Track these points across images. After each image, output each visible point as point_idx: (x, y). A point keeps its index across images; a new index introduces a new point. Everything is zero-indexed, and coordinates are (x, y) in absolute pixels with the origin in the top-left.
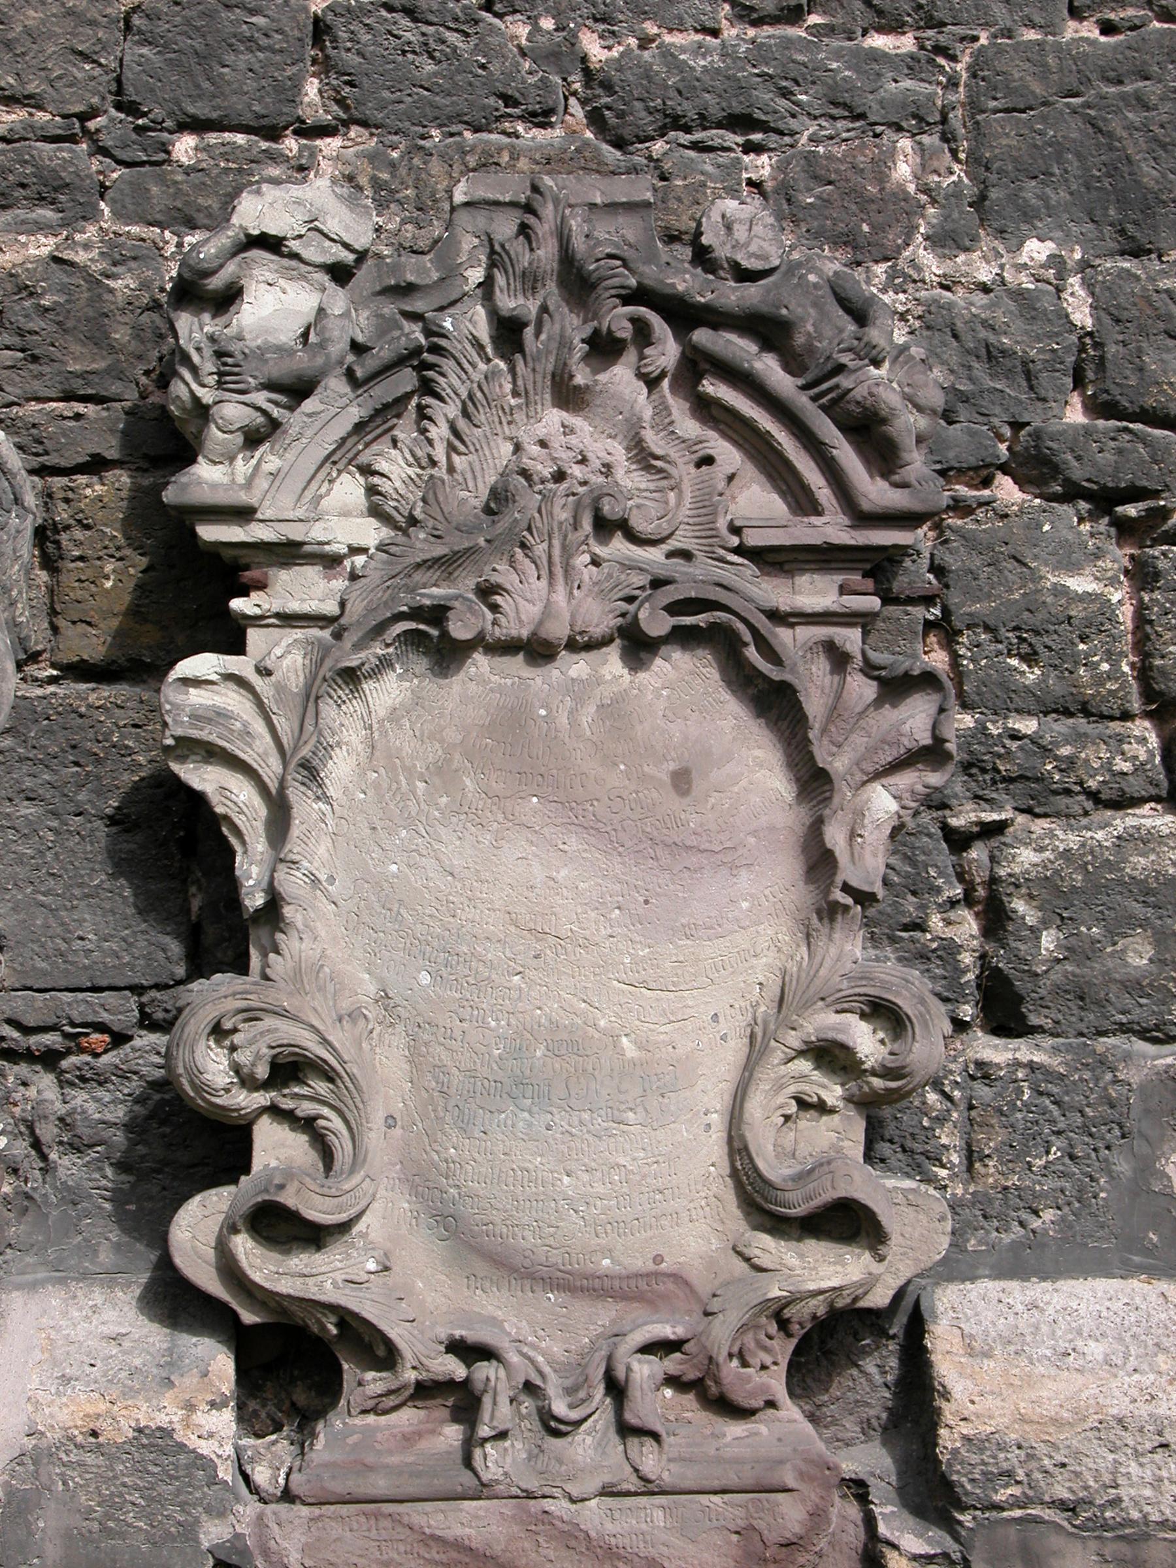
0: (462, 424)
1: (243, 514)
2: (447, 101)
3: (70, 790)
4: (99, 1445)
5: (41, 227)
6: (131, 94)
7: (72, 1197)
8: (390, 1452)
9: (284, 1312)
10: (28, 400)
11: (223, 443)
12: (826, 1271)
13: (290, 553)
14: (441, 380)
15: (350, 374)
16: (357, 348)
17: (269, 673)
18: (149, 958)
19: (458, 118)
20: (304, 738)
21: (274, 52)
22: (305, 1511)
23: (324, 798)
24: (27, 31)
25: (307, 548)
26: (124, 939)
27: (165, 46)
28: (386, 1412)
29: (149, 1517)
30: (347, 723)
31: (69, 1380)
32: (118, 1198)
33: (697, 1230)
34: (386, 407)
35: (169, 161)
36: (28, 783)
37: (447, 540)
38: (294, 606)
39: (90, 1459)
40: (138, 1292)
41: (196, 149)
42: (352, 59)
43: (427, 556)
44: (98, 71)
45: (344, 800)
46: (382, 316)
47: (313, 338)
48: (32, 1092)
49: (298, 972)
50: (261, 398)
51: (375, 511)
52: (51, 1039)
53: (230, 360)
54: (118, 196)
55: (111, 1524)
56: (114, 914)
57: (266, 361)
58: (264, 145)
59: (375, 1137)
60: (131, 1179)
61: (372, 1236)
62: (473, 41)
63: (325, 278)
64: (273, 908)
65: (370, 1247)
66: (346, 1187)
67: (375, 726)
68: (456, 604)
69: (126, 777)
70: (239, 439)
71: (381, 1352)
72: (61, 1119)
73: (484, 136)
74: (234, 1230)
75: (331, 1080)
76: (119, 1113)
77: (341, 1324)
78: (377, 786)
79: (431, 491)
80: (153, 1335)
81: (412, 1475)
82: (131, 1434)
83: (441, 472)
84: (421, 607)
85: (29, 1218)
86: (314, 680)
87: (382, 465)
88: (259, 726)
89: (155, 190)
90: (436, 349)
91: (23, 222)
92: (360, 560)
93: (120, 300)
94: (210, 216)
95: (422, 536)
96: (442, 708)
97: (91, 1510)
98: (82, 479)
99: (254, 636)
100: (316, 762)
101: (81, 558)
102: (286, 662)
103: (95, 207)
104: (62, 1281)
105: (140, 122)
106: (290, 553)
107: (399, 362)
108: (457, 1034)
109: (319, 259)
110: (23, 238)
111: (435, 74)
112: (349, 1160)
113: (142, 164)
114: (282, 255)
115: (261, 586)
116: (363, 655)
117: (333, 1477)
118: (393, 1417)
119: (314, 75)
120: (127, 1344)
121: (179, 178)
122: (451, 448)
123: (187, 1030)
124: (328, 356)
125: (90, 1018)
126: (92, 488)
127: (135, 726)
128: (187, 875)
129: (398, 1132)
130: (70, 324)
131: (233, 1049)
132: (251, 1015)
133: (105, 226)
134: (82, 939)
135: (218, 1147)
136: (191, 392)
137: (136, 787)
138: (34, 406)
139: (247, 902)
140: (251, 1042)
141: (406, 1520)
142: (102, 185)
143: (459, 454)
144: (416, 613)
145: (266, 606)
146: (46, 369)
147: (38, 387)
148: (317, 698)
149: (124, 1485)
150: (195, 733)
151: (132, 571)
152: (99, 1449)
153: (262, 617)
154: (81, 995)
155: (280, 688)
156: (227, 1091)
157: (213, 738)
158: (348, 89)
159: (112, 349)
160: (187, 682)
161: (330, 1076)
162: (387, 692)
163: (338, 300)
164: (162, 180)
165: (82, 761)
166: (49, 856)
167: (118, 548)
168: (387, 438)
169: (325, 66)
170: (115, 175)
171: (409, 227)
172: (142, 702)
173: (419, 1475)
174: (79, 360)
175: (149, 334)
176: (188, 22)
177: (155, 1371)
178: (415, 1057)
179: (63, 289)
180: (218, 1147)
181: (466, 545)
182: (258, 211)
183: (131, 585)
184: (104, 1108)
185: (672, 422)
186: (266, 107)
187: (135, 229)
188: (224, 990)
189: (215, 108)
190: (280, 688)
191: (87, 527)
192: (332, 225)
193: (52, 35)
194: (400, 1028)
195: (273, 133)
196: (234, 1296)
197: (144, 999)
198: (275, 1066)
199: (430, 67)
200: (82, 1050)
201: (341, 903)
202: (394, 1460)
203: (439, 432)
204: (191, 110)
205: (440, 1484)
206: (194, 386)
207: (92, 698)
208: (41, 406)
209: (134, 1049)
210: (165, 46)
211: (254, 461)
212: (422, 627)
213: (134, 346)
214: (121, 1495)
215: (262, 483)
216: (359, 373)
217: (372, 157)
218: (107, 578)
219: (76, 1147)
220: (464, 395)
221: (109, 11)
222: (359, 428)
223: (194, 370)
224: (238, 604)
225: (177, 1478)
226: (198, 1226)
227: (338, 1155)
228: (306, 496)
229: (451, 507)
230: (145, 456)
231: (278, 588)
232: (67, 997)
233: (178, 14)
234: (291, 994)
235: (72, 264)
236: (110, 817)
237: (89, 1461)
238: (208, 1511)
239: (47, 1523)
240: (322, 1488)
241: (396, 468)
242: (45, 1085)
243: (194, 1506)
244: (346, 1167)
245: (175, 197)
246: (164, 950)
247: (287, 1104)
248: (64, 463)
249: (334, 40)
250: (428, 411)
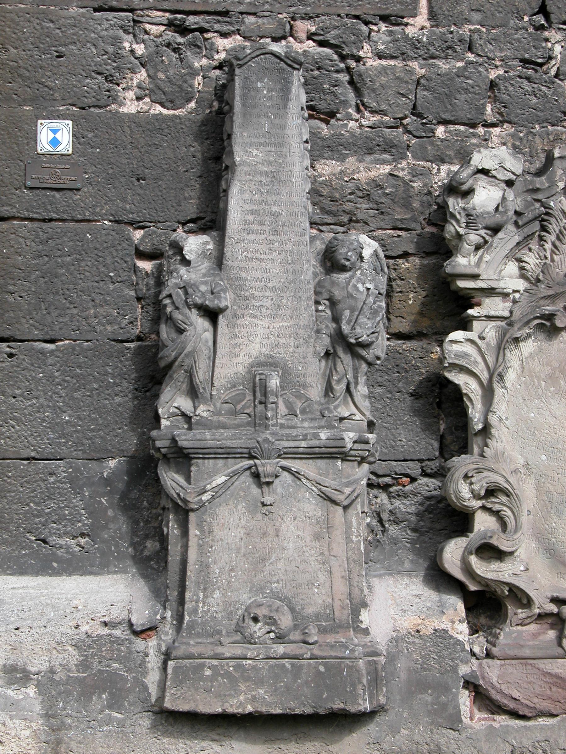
0: (558, 243)
1: (475, 277)
2: (542, 114)
3: (396, 382)
4: (420, 636)
5: (384, 162)
6: (420, 109)
7: (394, 541)
8: (529, 640)
9: (487, 585)
10: (378, 229)
11: (468, 250)
13: (491, 292)
14: (550, 226)
15: (516, 223)
16: (517, 213)
17: (484, 339)
18: (426, 448)
19: (546, 121)
20: (499, 364)
21: (475, 94)
22: (499, 662)
23: (505, 387)
24: (382, 86)
25: (497, 290)
26: (416, 441)
27: (434, 91)
28: (525, 625)
29: (440, 664)
30: (513, 357)
31: (405, 611)
32: (413, 542)
34: (528, 236)
35: (434, 137)
36: (380, 379)
37: (554, 288)
38: (492, 313)
39: (417, 641)
40: (421, 579)
41: (445, 132)
42: (506, 97)
43: (546, 295)
44: (408, 101)
45: (512, 388)
46: (527, 201)
47: (501, 209)
48: (379, 500)
49: (496, 454)
50: (483, 232)
51: (523, 276)
52: (387, 480)
53: (472, 218)
54: (414, 150)
55: (425, 666)
56: (413, 431)
57: (485, 218)
58: (471, 130)
59: (524, 519)
60: (417, 535)
61: (522, 557)
62: (552, 90)
63: (503, 185)
64: (486, 431)
65: (521, 561)
66: (515, 537)
67: (524, 360)
68: (558, 313)
69: (417, 378)
70: (473, 248)
71: (525, 601)
72: (390, 511)
73: (556, 128)
74: (471, 554)
75: (508, 496)
76: (413, 509)
77: (510, 591)
78: (525, 383)
79: (545, 269)
80: (430, 596)
81: (538, 649)
82: (432, 632)
83: (548, 261)
84: (544, 315)
85: (378, 549)
86: (502, 341)
87: (526, 259)
88: (479, 359)
89: (429, 148)
90: (547, 214)
91: (378, 160)
92: (517, 295)
93: (416, 191)
94: (450, 158)
95: (543, 286)
96: (550, 353)
97: (418, 660)
98: (401, 261)
99: (475, 324)
100: (503, 374)
101: (400, 292)
102: (489, 334)
103: (406, 154)
104: (391, 574)
105: (424, 121)
106: (491, 292)
107: (535, 219)
108: (556, 479)
109: (503, 178)
110: (378, 166)
111: (537, 103)
112: (514, 527)
113: (423, 137)
114: (489, 176)
115: (479, 305)
116: (521, 332)
117: (509, 649)
118: (528, 627)
119: (489, 102)
120: (423, 598)
121: (439, 143)
122: (553, 252)
123: (454, 476)
124: (508, 216)
125: (403, 472)
126: (404, 264)
127: (421, 358)
129: (531, 517)
130: (396, 200)
131: (471, 484)
132: (479, 471)
133: (410, 161)
134: (400, 441)
135: (461, 522)
136: (456, 229)
137: (421, 382)
138: (380, 232)
139: (475, 427)
140: (480, 481)
141: (537, 666)
142: (408, 146)
143: (556, 255)
144: (542, 317)
145: (481, 313)
146: (386, 217)
147: (382, 224)
148: (504, 349)
149: (430, 651)
150: (457, 362)
151: (420, 297)
152: (420, 637)
153: (480, 317)
154: (399, 463)
155: (488, 345)
156: (469, 500)
157: (464, 364)
158: (503, 109)
159: (412, 210)
160: (452, 341)
161: (507, 494)
162: (529, 347)
163: (510, 195)
164: (432, 144)
165: (400, 371)
166: (388, 408)
167: (415, 288)
168: (527, 248)
169: (495, 99)
170: (413, 142)
171: (527, 163)
172: (423, 348)
173: (541, 649)
174: (400, 214)
175: (426, 204)
176: (443, 82)
177: (437, 608)
178: (538, 488)
179: (394, 186)
180: (461, 522)
181: (561, 290)
182: (479, 159)
183: (419, 303)
184: (407, 507)
186: (472, 116)
187: (421, 163)
188: (468, 461)
189: (452, 116)
190: (488, 345)
191: (403, 280)
192: (508, 165)
193: (390, 87)
194: (533, 477)
195: (473, 126)
196: (468, 580)
197: (423, 464)
198: (487, 490)
199: (535, 100)
200: (399, 484)
201: (510, 428)
202: (531, 643)
203: (548, 246)
204: (444, 117)
205: (549, 652)
206: (457, 227)
207: (404, 346)
208: (384, 232)
209: (419, 484)
210: (434, 91)
211: (478, 257)
212: (543, 322)
213: (420, 209)
214: (429, 655)
215: (483, 265)
216: (520, 223)
217: (513, 136)
218: (410, 300)
219: (396, 522)
220: (557, 232)
221: (413, 77)
222: (518, 243)
223: (458, 221)
224: (470, 312)
225: (450, 649)
226: (453, 553)
227: (509, 525)
228: (494, 269)
229: (554, 275)
230: (424, 252)
231: (485, 305)
232: (394, 463)
233: (439, 79)
234: (494, 463)
235: (398, 176)
236: (411, 393)
237: (417, 642)
238: (462, 661)
239: (401, 665)
240: (505, 653)
241: (532, 260)
242: (383, 497)
243: (456, 659)
244: (513, 530)
245: (437, 150)
246: (432, 446)
247: (489, 506)
248: (394, 255)
249: (499, 89)
250: (544, 238)
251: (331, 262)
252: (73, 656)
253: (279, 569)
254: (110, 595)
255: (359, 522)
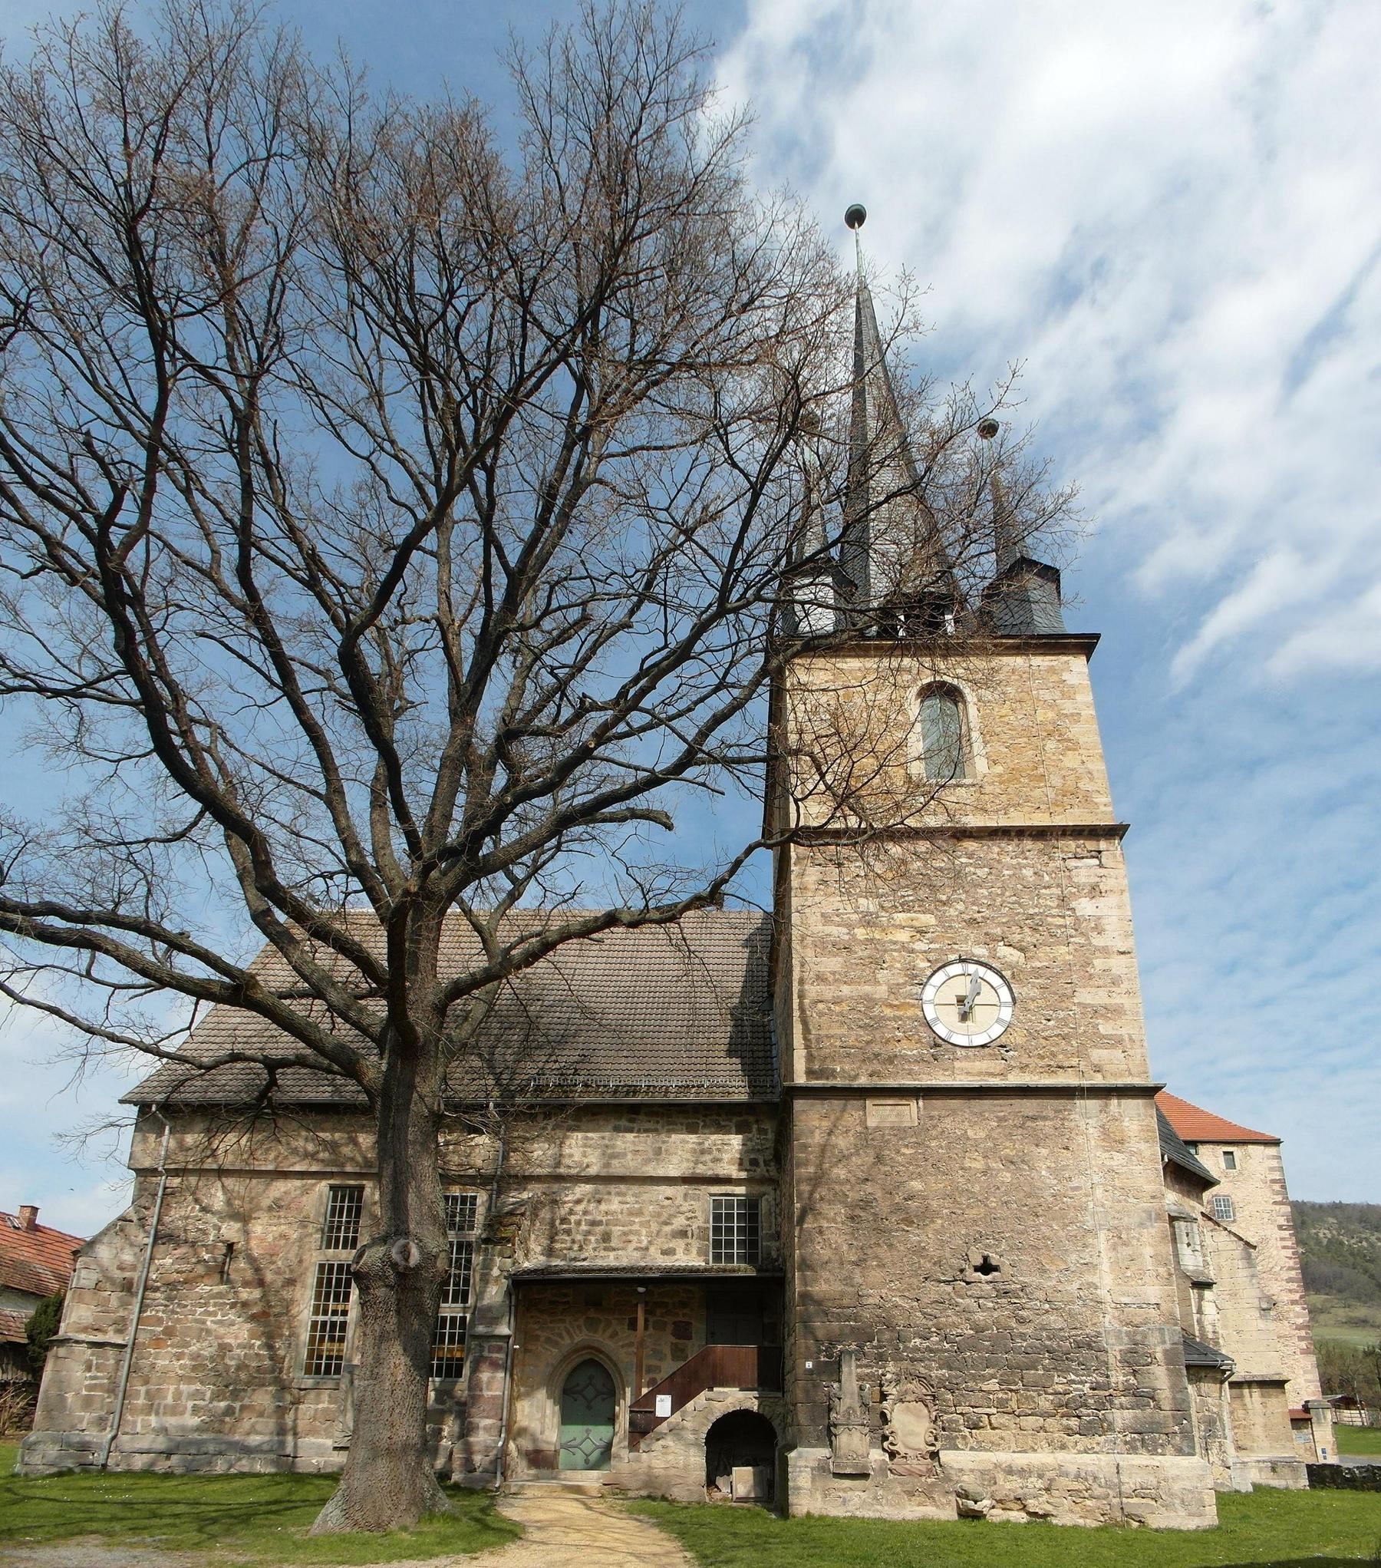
12: (932, 1448)
33: (923, 1446)
128: (884, 1419)
185: (129, 32)
226: (886, 1444)
228: (892, 1390)
251: (861, 1389)
252: (1210, 1517)
253: (853, 1447)
254: (825, 1452)
255: (868, 1438)
